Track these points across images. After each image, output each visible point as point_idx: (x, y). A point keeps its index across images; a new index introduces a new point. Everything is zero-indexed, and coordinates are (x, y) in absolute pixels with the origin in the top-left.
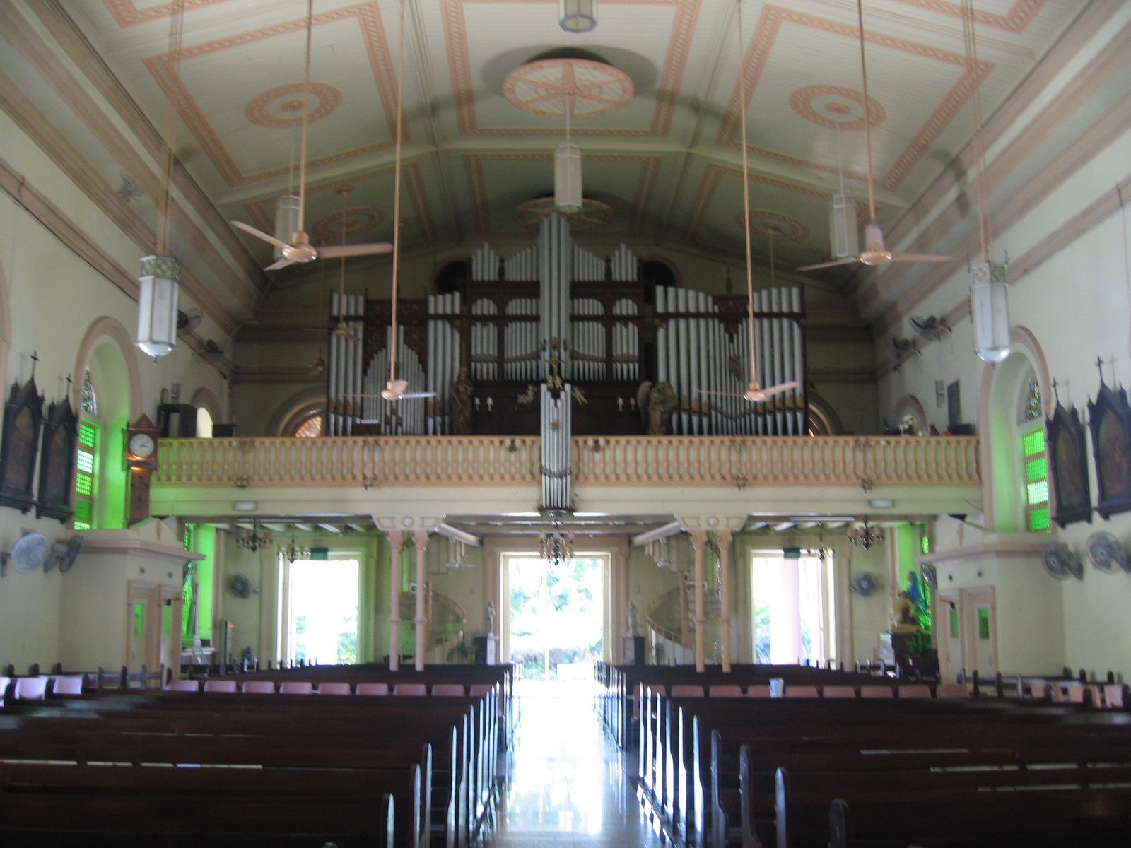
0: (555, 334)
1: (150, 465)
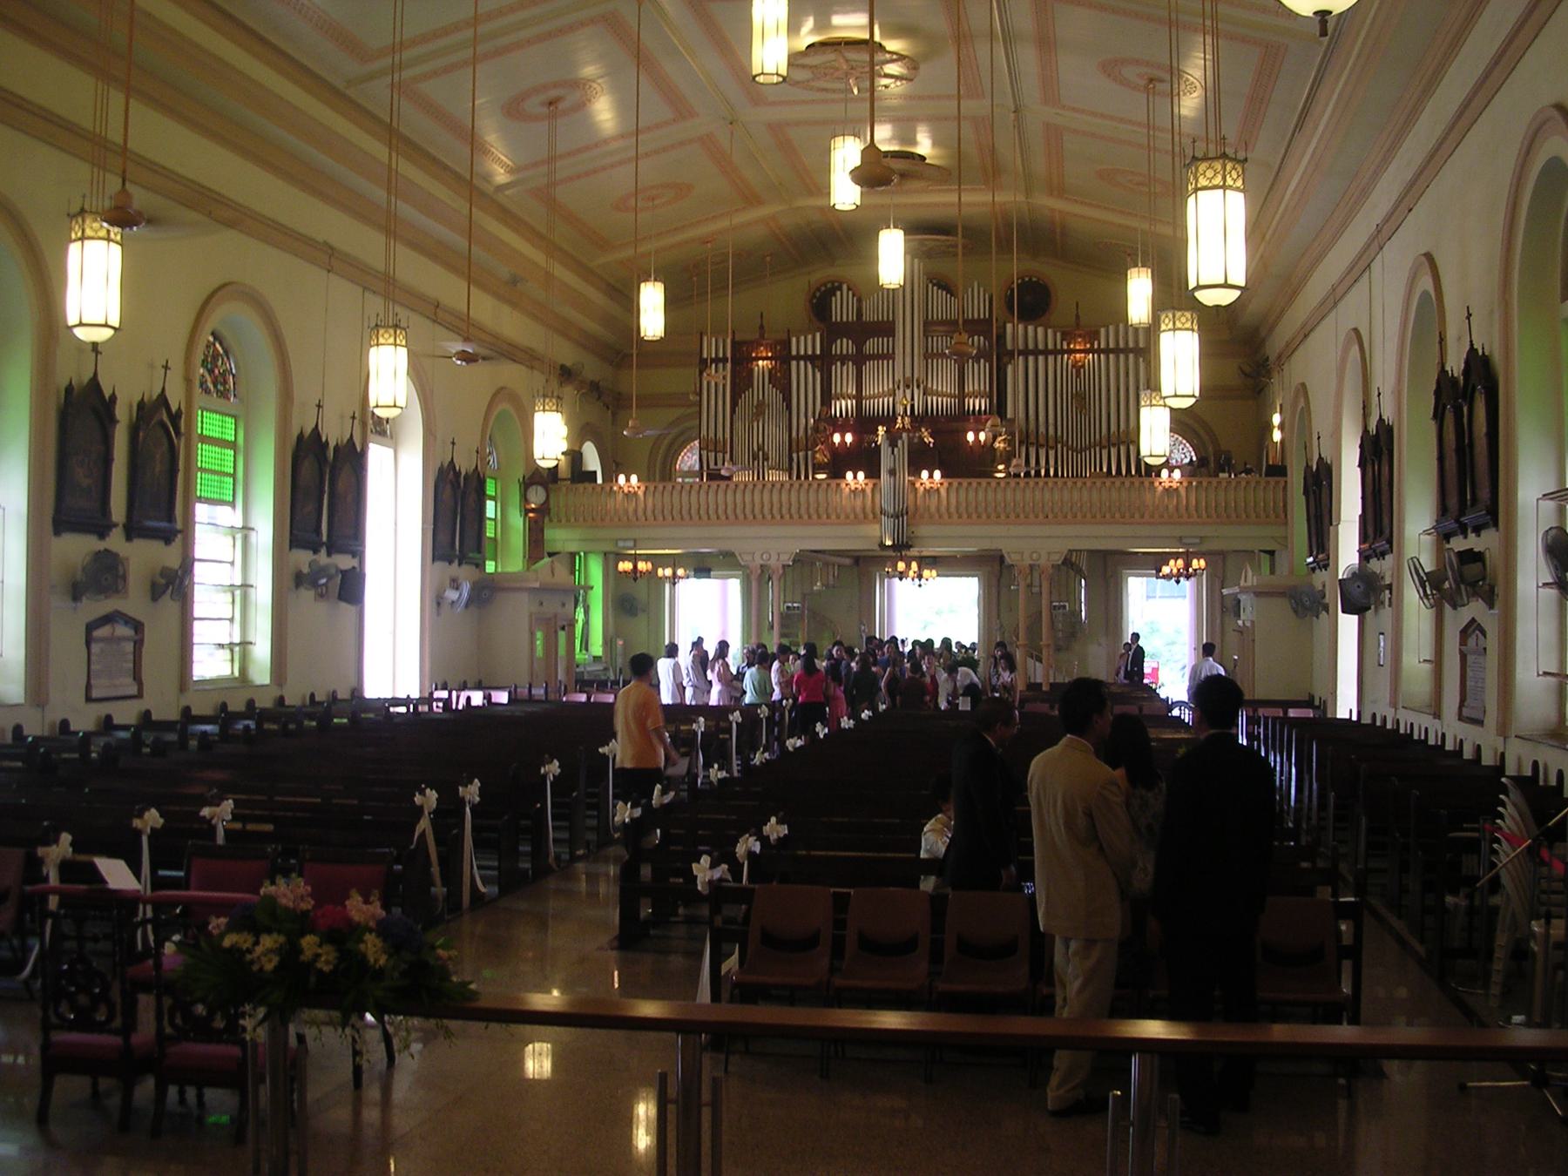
0: (908, 374)
1: (543, 510)
